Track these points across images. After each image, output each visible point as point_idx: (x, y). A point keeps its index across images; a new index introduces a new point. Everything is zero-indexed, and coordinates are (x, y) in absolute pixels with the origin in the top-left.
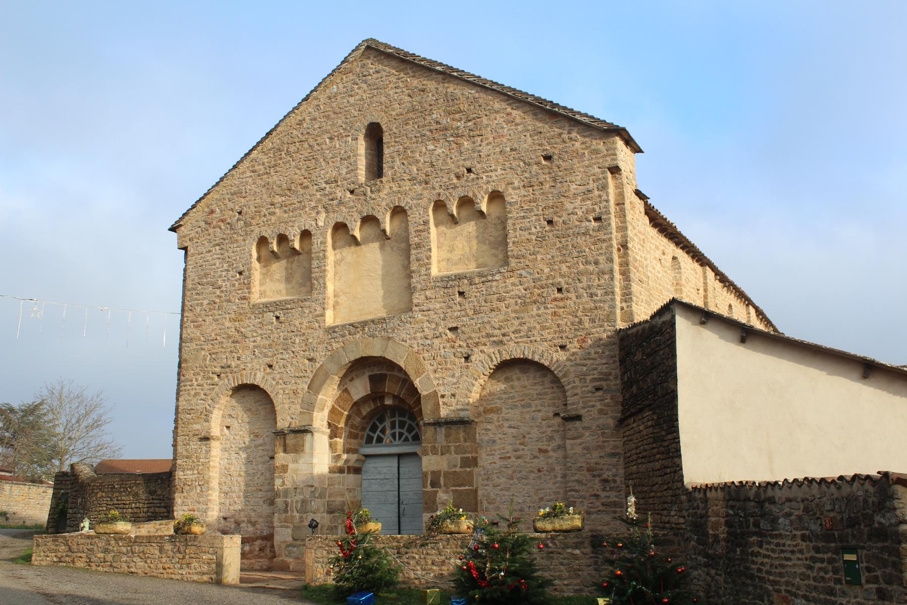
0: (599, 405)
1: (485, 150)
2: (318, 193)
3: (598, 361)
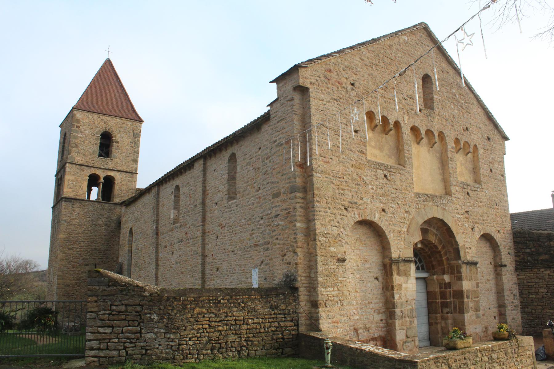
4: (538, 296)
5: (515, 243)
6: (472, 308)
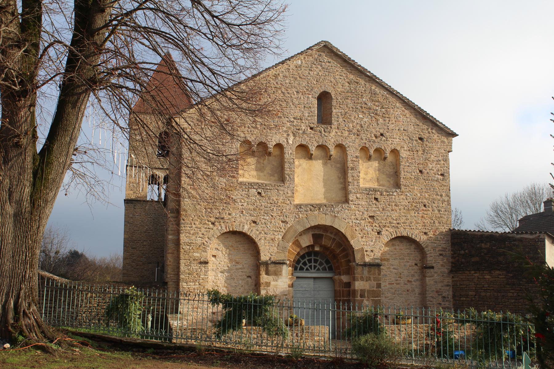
0: (441, 262)
1: (391, 127)
4: (468, 299)
5: (453, 244)
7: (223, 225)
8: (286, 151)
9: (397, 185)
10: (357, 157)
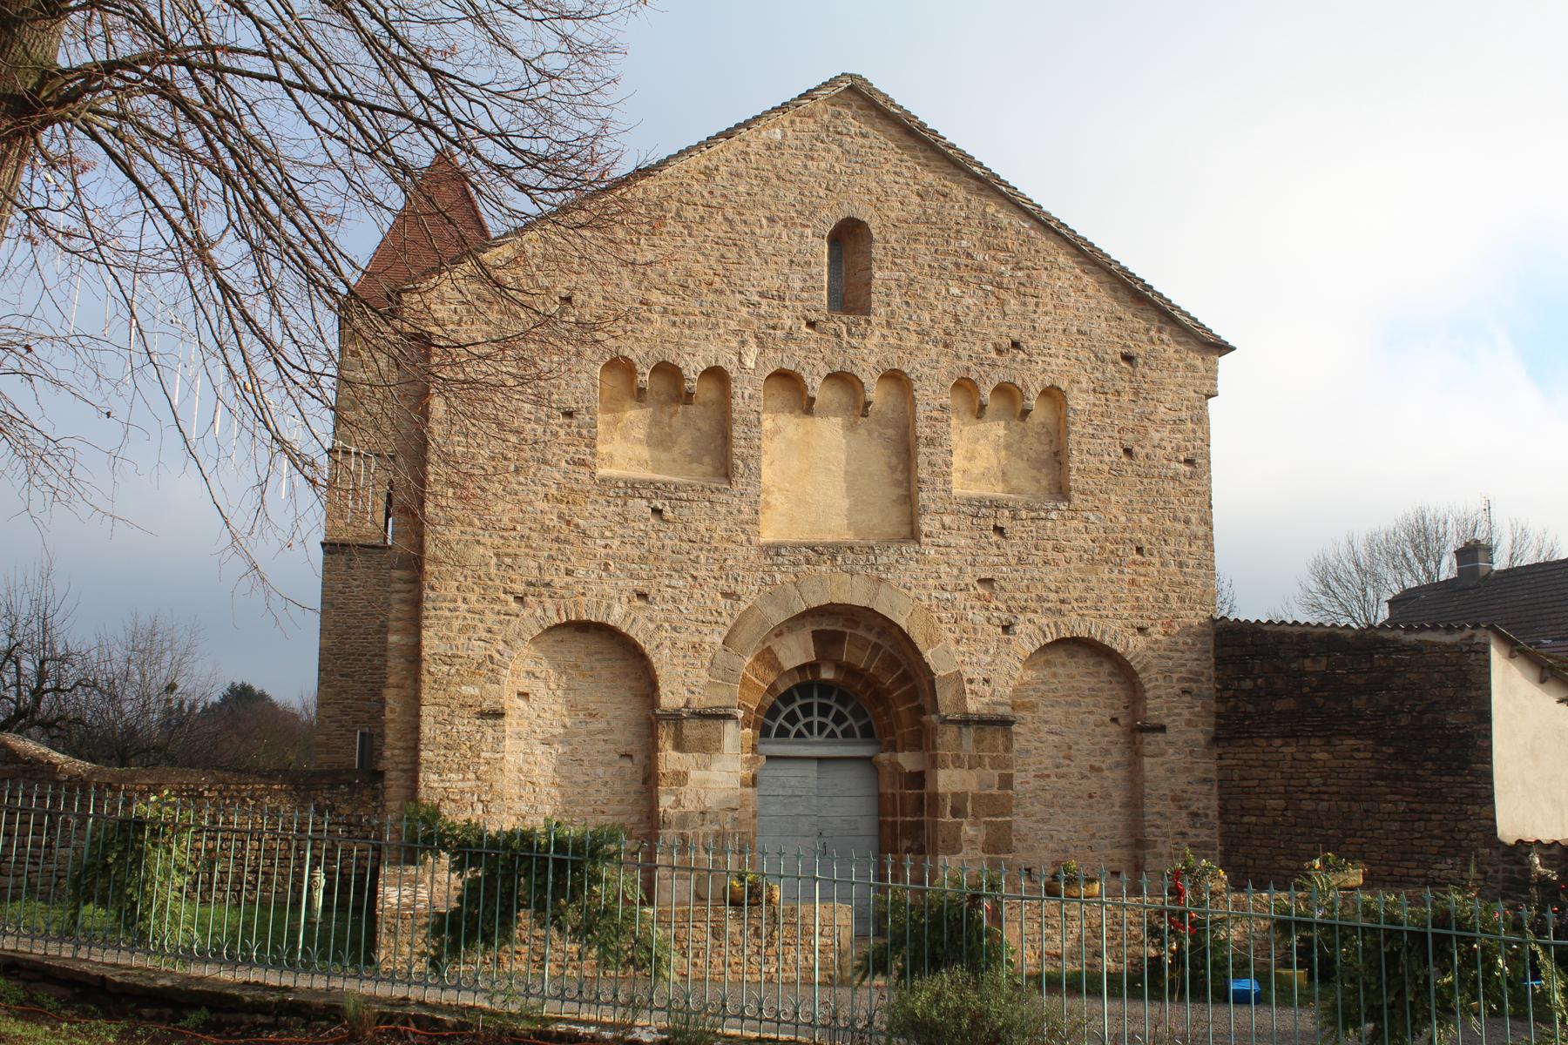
0: (1187, 714)
1: (1043, 322)
2: (745, 309)
3: (1188, 655)
4: (1264, 820)
5: (1220, 661)
6: (972, 842)
7: (549, 603)
8: (736, 388)
9: (1061, 491)
10: (943, 408)
